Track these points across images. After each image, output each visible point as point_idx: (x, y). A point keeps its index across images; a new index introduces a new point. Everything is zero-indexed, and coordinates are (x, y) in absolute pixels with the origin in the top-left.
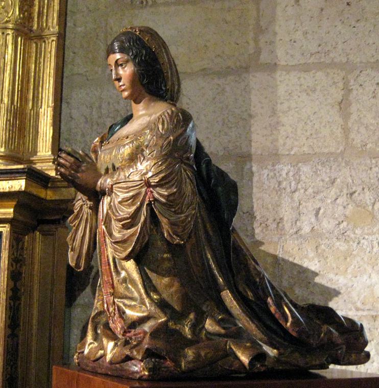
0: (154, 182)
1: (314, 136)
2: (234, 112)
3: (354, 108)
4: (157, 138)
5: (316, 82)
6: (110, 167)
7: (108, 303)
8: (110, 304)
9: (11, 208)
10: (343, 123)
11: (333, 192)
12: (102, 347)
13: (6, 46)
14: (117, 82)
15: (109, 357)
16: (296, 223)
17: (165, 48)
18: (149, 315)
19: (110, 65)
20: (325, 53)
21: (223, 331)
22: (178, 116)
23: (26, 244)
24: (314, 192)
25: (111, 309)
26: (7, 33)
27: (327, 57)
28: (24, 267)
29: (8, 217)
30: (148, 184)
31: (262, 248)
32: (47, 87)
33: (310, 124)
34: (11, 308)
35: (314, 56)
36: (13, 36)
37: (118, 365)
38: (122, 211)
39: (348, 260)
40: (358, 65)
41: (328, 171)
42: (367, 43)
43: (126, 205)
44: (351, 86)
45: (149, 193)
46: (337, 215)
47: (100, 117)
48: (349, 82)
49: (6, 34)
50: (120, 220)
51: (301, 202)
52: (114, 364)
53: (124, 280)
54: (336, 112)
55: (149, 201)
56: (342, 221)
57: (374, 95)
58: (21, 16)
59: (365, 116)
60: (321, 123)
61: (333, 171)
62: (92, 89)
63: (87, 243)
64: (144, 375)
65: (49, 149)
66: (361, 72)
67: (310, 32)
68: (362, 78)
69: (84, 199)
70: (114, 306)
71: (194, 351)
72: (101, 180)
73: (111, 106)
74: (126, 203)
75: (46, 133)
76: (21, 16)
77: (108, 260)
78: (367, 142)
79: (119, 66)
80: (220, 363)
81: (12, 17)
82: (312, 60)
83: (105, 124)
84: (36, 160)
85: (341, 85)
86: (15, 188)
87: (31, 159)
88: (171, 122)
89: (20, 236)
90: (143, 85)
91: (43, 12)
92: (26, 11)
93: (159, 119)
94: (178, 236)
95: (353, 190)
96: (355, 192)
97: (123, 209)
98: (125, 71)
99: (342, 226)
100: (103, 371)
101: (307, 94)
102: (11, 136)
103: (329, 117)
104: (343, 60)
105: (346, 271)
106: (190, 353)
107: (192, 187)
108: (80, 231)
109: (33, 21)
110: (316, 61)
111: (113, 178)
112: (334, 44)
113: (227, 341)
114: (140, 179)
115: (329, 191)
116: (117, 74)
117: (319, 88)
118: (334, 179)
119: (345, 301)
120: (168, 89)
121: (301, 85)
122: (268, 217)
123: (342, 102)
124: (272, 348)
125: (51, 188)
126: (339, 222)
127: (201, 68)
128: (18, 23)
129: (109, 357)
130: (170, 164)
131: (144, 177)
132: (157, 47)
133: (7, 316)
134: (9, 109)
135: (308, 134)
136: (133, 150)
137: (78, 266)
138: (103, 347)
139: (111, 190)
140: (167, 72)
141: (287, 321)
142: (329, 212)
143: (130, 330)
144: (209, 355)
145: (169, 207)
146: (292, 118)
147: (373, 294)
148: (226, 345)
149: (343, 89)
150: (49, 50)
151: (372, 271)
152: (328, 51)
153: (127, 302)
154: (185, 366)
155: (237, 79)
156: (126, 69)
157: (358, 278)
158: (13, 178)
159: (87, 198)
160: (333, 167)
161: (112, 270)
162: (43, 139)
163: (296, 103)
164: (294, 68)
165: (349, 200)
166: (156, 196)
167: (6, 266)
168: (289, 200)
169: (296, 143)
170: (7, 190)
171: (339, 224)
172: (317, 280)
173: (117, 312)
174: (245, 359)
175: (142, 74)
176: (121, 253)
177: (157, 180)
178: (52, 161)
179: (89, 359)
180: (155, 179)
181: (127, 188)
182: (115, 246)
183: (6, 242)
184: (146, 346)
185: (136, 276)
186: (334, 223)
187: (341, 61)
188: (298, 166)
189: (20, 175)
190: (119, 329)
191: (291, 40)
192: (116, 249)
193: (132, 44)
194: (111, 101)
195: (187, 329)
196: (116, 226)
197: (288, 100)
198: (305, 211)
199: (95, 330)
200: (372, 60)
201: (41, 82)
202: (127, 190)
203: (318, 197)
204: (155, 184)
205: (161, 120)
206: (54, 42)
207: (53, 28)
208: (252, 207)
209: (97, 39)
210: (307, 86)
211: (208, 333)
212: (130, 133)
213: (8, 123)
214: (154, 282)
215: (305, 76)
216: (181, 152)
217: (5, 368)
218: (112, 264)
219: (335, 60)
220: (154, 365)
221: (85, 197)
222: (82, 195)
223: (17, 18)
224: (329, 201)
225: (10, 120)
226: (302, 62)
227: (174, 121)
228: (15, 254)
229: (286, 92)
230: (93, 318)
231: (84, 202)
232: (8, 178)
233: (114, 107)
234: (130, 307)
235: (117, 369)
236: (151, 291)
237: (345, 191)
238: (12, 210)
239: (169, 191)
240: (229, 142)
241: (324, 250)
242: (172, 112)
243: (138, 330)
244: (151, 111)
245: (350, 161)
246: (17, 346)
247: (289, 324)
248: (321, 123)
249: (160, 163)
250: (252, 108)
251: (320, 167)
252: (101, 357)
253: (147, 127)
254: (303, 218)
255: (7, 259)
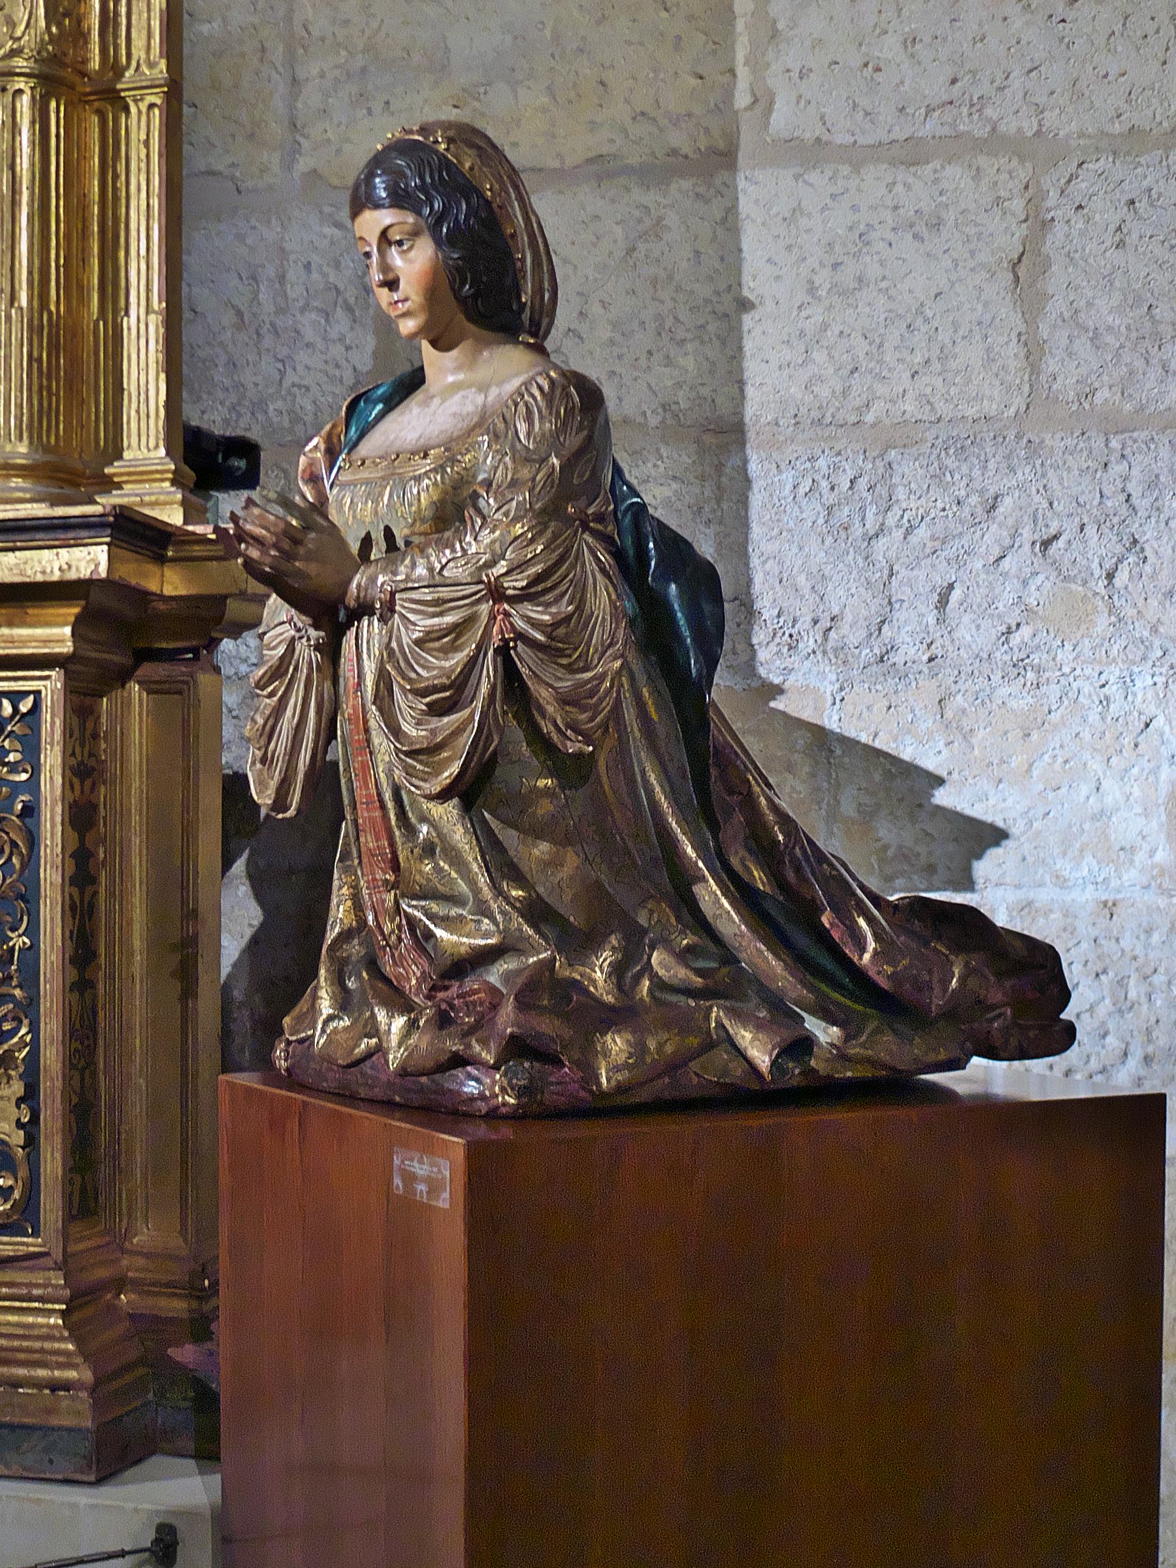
0: (514, 588)
1: (936, 366)
2: (692, 292)
3: (1057, 278)
4: (514, 460)
5: (944, 199)
6: (378, 536)
7: (379, 908)
8: (386, 911)
9: (65, 624)
10: (1022, 328)
11: (992, 537)
12: (373, 1030)
13: (15, 129)
14: (386, 290)
15: (395, 1058)
16: (880, 630)
17: (516, 188)
18: (501, 944)
19: (361, 238)
20: (972, 105)
21: (698, 981)
22: (568, 396)
23: (104, 720)
24: (933, 538)
25: (387, 927)
26: (17, 87)
27: (976, 117)
28: (103, 789)
29: (57, 650)
30: (496, 593)
31: (778, 704)
32: (143, 252)
33: (924, 329)
34: (73, 908)
35: (936, 114)
36: (33, 97)
37: (424, 1079)
38: (423, 667)
39: (1035, 736)
40: (1073, 143)
41: (976, 473)
42: (1102, 73)
43: (440, 650)
44: (1049, 210)
45: (500, 617)
46: (1001, 606)
47: (281, 311)
48: (1044, 195)
49: (11, 92)
50: (422, 693)
51: (895, 568)
52: (412, 1075)
53: (429, 850)
54: (1003, 293)
55: (503, 639)
56: (1018, 625)
57: (1117, 239)
58: (54, 29)
59: (1089, 304)
60: (956, 326)
61: (991, 474)
62: (253, 222)
63: (310, 745)
64: (504, 1104)
65: (157, 438)
66: (1080, 165)
67: (927, 39)
68: (1083, 185)
69: (300, 625)
70: (398, 918)
71: (630, 1037)
72: (358, 576)
73: (315, 276)
74: (437, 644)
75: (147, 390)
76: (54, 29)
77: (379, 795)
78: (1096, 385)
79: (390, 243)
80: (694, 1065)
81: (26, 38)
82: (929, 128)
83: (297, 332)
84: (122, 474)
85: (1017, 205)
86: (77, 569)
87: (106, 471)
88: (551, 413)
89: (88, 701)
90: (461, 301)
91: (117, 14)
92: (66, 14)
93: (516, 405)
94: (577, 731)
95: (1053, 531)
96: (1056, 537)
97: (427, 660)
98: (410, 261)
99: (1016, 639)
100: (378, 1093)
101: (916, 236)
102: (45, 404)
103: (980, 307)
104: (1025, 124)
105: (1029, 770)
106: (617, 1044)
107: (614, 597)
108: (289, 712)
109: (86, 42)
110: (946, 131)
111: (395, 573)
112: (999, 77)
113: (711, 1007)
114: (474, 580)
115: (979, 533)
116: (385, 267)
117: (950, 216)
118: (996, 498)
119: (1024, 859)
120: (525, 304)
121: (896, 208)
122: (798, 613)
123: (1020, 260)
124: (828, 1022)
125: (173, 560)
126: (1009, 628)
127: (590, 155)
128: (45, 54)
129: (395, 1058)
130: (555, 537)
131: (487, 576)
132: (497, 186)
133: (67, 933)
134: (36, 322)
135: (918, 358)
136: (445, 492)
137: (280, 803)
138: (377, 1030)
139: (390, 607)
140: (523, 260)
141: (862, 949)
142: (978, 597)
143: (447, 983)
144: (669, 1049)
145: (555, 656)
146: (867, 310)
147: (1107, 837)
148: (707, 1018)
149: (1025, 221)
150: (143, 137)
151: (1104, 773)
152: (981, 98)
153: (434, 907)
154: (608, 1080)
155: (701, 190)
156: (412, 254)
157: (1063, 790)
158: (72, 542)
159: (308, 620)
160: (992, 465)
161: (393, 822)
162: (138, 412)
163: (882, 263)
164: (878, 152)
165: (1038, 561)
166: (520, 624)
167: (58, 792)
168: (860, 561)
169: (881, 389)
170: (56, 576)
171: (1009, 631)
172: (942, 797)
173: (406, 936)
174: (762, 1059)
175: (458, 269)
176: (425, 781)
177: (524, 583)
178: (170, 476)
179: (331, 1061)
180: (516, 580)
181: (437, 602)
182: (408, 760)
183: (53, 723)
184: (509, 1030)
185: (460, 836)
186: (992, 630)
187: (1020, 130)
188: (887, 458)
189: (92, 533)
190: (414, 982)
191: (866, 65)
192: (410, 770)
193: (428, 180)
194: (315, 259)
195: (598, 975)
196: (407, 708)
197: (857, 255)
198: (905, 593)
199: (339, 980)
200: (1117, 128)
201: (122, 234)
202: (438, 609)
203: (949, 552)
204: (517, 592)
205: (522, 408)
206: (157, 111)
207: (151, 65)
208: (749, 582)
209: (262, 60)
210: (916, 212)
211: (659, 985)
212: (432, 443)
213: (35, 365)
214: (512, 853)
215: (910, 180)
216: (582, 502)
217: (68, 1078)
218: (390, 805)
219: (1002, 128)
220: (531, 1079)
221: (304, 618)
222: (293, 611)
223: (42, 40)
224: (979, 565)
225: (40, 360)
226: (899, 134)
227: (558, 413)
228: (78, 750)
229: (851, 228)
230: (331, 948)
231: (299, 630)
232: (57, 543)
233: (325, 275)
234: (444, 921)
235: (422, 1089)
236: (503, 879)
237: (1027, 534)
238: (68, 630)
239: (554, 610)
240: (679, 385)
241: (964, 711)
242: (552, 382)
243: (471, 983)
244: (483, 372)
245: (1043, 441)
246: (95, 1014)
247: (867, 957)
248: (956, 326)
249: (530, 535)
250: (747, 279)
251: (950, 462)
252: (369, 1055)
253: (478, 425)
254: (900, 615)
255: (60, 771)
